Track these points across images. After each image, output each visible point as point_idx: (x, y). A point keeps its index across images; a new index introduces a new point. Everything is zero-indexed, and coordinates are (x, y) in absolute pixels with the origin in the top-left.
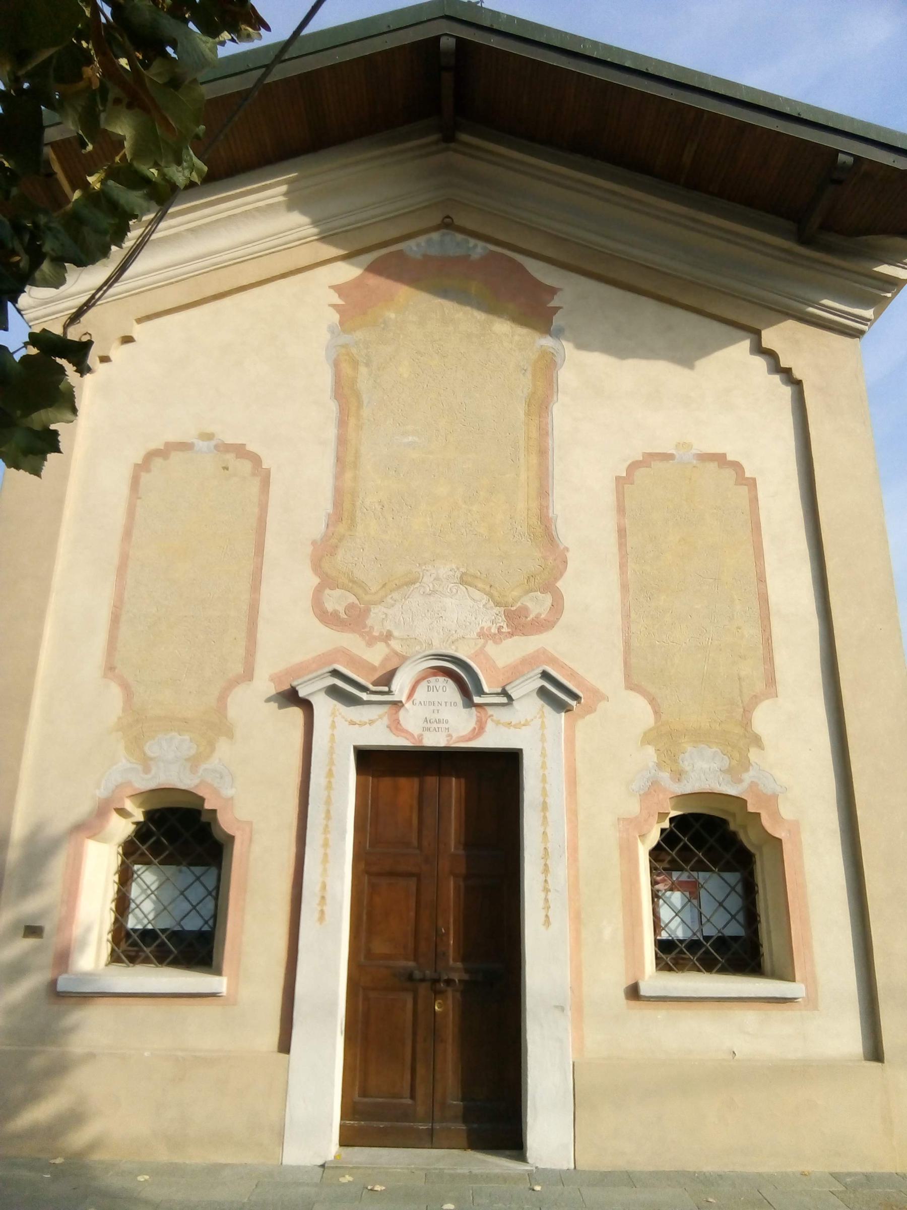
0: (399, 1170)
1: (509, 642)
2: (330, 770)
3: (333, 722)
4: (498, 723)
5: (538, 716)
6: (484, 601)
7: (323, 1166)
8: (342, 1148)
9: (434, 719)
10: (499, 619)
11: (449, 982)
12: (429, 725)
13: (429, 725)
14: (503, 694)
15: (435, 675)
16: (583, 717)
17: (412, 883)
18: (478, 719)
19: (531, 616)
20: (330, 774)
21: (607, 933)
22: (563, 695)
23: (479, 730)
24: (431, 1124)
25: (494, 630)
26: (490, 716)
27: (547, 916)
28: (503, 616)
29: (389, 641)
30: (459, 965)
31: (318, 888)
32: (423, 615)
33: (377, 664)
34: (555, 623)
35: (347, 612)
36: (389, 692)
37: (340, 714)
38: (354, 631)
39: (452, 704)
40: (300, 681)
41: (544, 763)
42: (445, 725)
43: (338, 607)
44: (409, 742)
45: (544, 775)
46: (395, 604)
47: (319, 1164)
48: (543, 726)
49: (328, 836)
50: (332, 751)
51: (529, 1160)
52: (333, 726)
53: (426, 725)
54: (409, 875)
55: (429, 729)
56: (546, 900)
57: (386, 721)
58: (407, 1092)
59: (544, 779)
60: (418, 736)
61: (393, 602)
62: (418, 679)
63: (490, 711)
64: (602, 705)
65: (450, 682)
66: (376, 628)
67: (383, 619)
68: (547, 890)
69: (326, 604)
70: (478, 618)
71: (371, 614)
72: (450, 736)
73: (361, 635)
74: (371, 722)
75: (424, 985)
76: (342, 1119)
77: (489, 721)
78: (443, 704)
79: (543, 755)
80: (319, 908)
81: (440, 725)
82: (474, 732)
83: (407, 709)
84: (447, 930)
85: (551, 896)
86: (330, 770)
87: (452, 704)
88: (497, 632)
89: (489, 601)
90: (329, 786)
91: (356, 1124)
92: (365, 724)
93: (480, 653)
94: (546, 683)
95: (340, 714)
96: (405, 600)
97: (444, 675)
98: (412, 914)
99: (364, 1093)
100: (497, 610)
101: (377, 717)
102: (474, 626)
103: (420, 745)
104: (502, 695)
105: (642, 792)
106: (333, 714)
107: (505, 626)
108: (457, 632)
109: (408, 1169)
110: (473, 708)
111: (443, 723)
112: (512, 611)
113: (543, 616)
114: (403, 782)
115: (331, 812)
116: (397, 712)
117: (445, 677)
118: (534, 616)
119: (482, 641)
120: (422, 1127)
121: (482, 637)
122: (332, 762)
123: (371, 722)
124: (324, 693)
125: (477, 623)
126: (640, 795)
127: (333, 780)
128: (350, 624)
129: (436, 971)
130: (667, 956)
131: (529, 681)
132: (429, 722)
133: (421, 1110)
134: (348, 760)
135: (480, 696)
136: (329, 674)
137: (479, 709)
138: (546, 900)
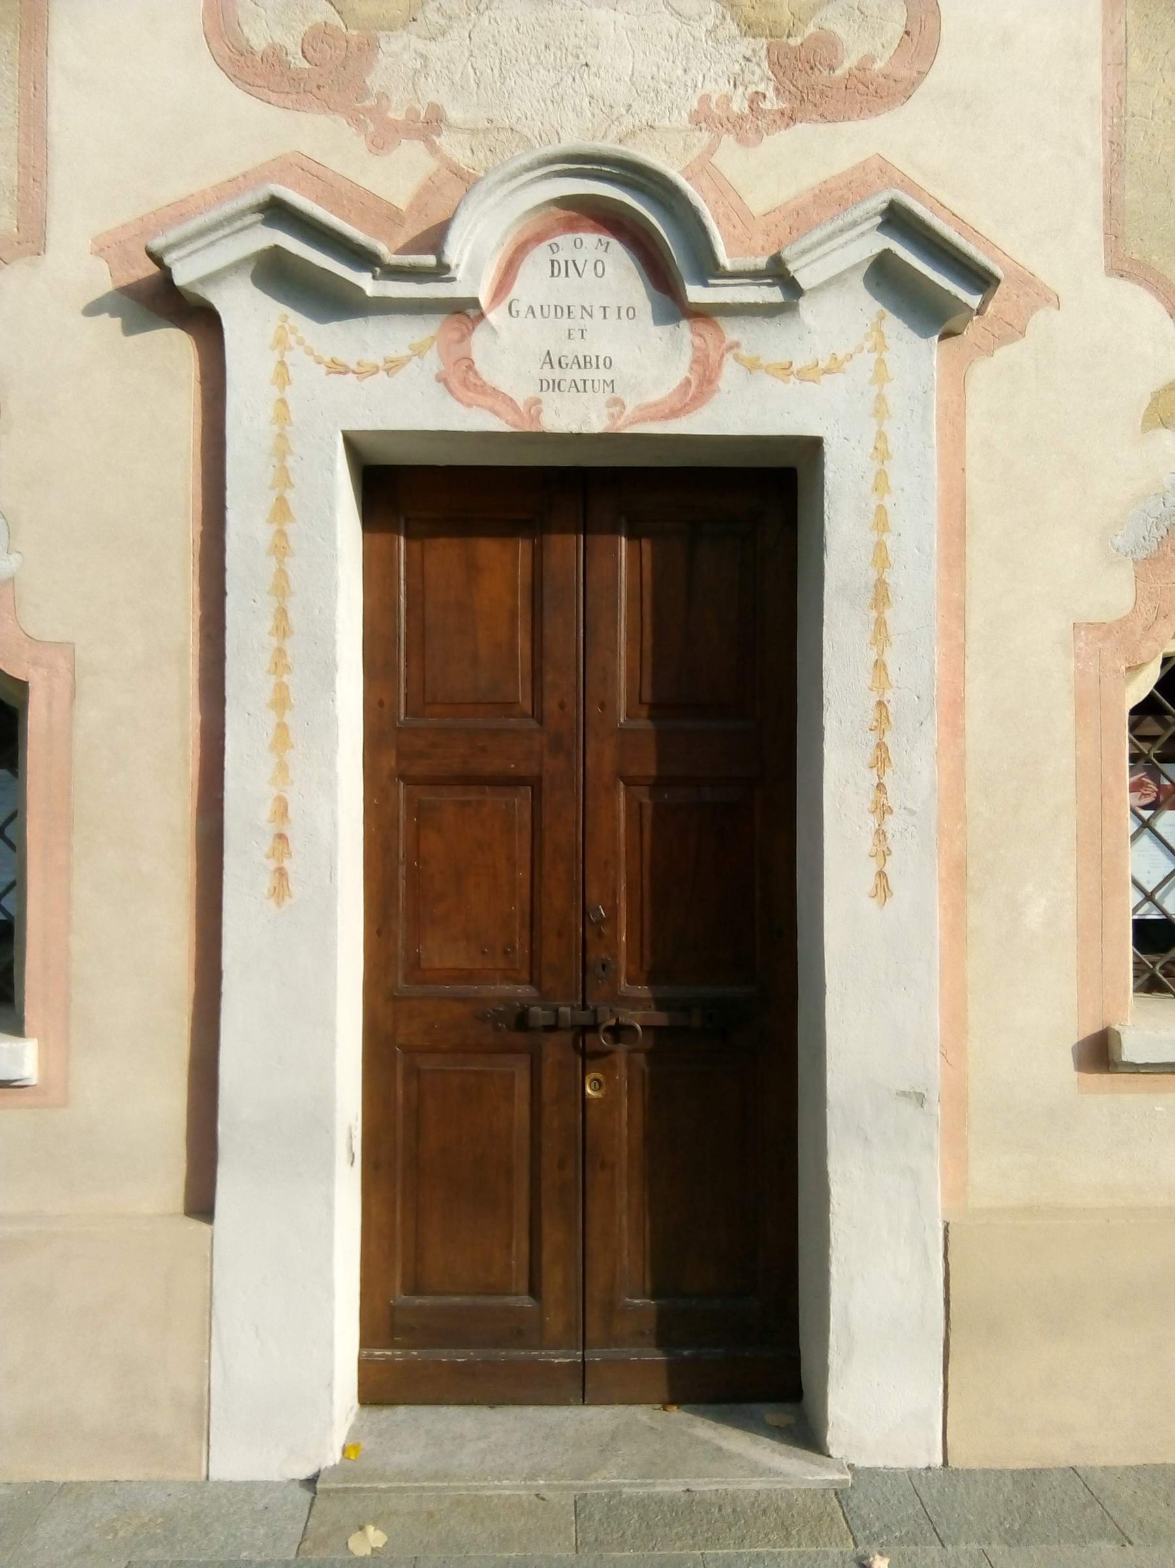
0: (508, 1492)
1: (782, 140)
2: (281, 501)
3: (282, 363)
4: (752, 366)
5: (868, 345)
6: (709, 21)
7: (311, 1483)
8: (367, 1409)
9: (571, 358)
10: (753, 73)
11: (618, 1032)
12: (557, 373)
13: (557, 373)
14: (768, 277)
15: (570, 226)
16: (990, 353)
17: (521, 801)
18: (697, 354)
19: (849, 63)
20: (281, 511)
21: (1035, 913)
22: (942, 277)
23: (700, 385)
24: (580, 1353)
25: (739, 105)
26: (730, 348)
27: (881, 874)
28: (765, 65)
29: (434, 137)
30: (643, 991)
31: (266, 811)
32: (533, 60)
33: (402, 202)
34: (914, 84)
35: (310, 53)
36: (441, 272)
37: (301, 342)
38: (329, 107)
39: (623, 313)
40: (172, 236)
41: (882, 475)
42: (602, 374)
43: (280, 37)
44: (503, 422)
45: (880, 508)
46: (451, 27)
47: (303, 1477)
48: (880, 374)
49: (285, 678)
50: (282, 449)
51: (834, 1438)
52: (282, 375)
53: (549, 374)
54: (511, 782)
55: (557, 385)
56: (881, 834)
57: (433, 361)
58: (524, 1284)
59: (881, 521)
60: (526, 403)
61: (443, 22)
62: (522, 239)
63: (733, 330)
64: (1040, 320)
65: (616, 245)
66: (395, 99)
67: (416, 71)
68: (882, 810)
69: (246, 29)
70: (694, 71)
71: (381, 55)
72: (618, 402)
73: (355, 120)
74: (392, 366)
75: (554, 1037)
76: (364, 1343)
77: (729, 362)
78: (598, 313)
79: (881, 452)
80: (272, 865)
81: (589, 374)
82: (686, 393)
83: (493, 329)
84: (613, 910)
85: (892, 824)
86: (281, 501)
87: (623, 313)
88: (747, 111)
89: (724, 18)
90: (280, 547)
91: (400, 1356)
92: (375, 370)
93: (703, 167)
94: (893, 241)
95: (301, 342)
96: (480, 13)
97: (599, 226)
98: (523, 874)
99: (415, 1287)
100: (745, 46)
101: (410, 352)
102: (682, 92)
103: (534, 430)
104: (769, 281)
105: (1142, 555)
106: (280, 342)
107: (770, 94)
108: (633, 110)
109: (528, 1488)
110: (684, 325)
111: (598, 367)
112: (790, 48)
113: (879, 65)
114: (488, 549)
115: (291, 615)
116: (464, 337)
117: (600, 232)
118: (856, 63)
119: (706, 137)
120: (560, 1359)
121: (703, 125)
122: (283, 478)
123: (392, 366)
124: (249, 280)
125: (689, 84)
126: (1135, 562)
127: (289, 528)
128: (319, 87)
129: (584, 1007)
130: (1154, 958)
131: (847, 236)
132: (556, 365)
133: (555, 1322)
134: (332, 471)
135: (706, 285)
136: (260, 216)
137: (701, 326)
138: (881, 834)
